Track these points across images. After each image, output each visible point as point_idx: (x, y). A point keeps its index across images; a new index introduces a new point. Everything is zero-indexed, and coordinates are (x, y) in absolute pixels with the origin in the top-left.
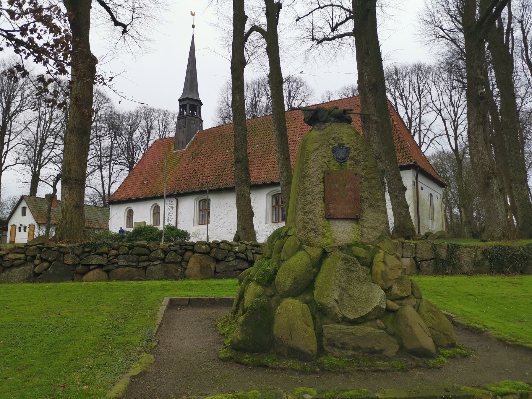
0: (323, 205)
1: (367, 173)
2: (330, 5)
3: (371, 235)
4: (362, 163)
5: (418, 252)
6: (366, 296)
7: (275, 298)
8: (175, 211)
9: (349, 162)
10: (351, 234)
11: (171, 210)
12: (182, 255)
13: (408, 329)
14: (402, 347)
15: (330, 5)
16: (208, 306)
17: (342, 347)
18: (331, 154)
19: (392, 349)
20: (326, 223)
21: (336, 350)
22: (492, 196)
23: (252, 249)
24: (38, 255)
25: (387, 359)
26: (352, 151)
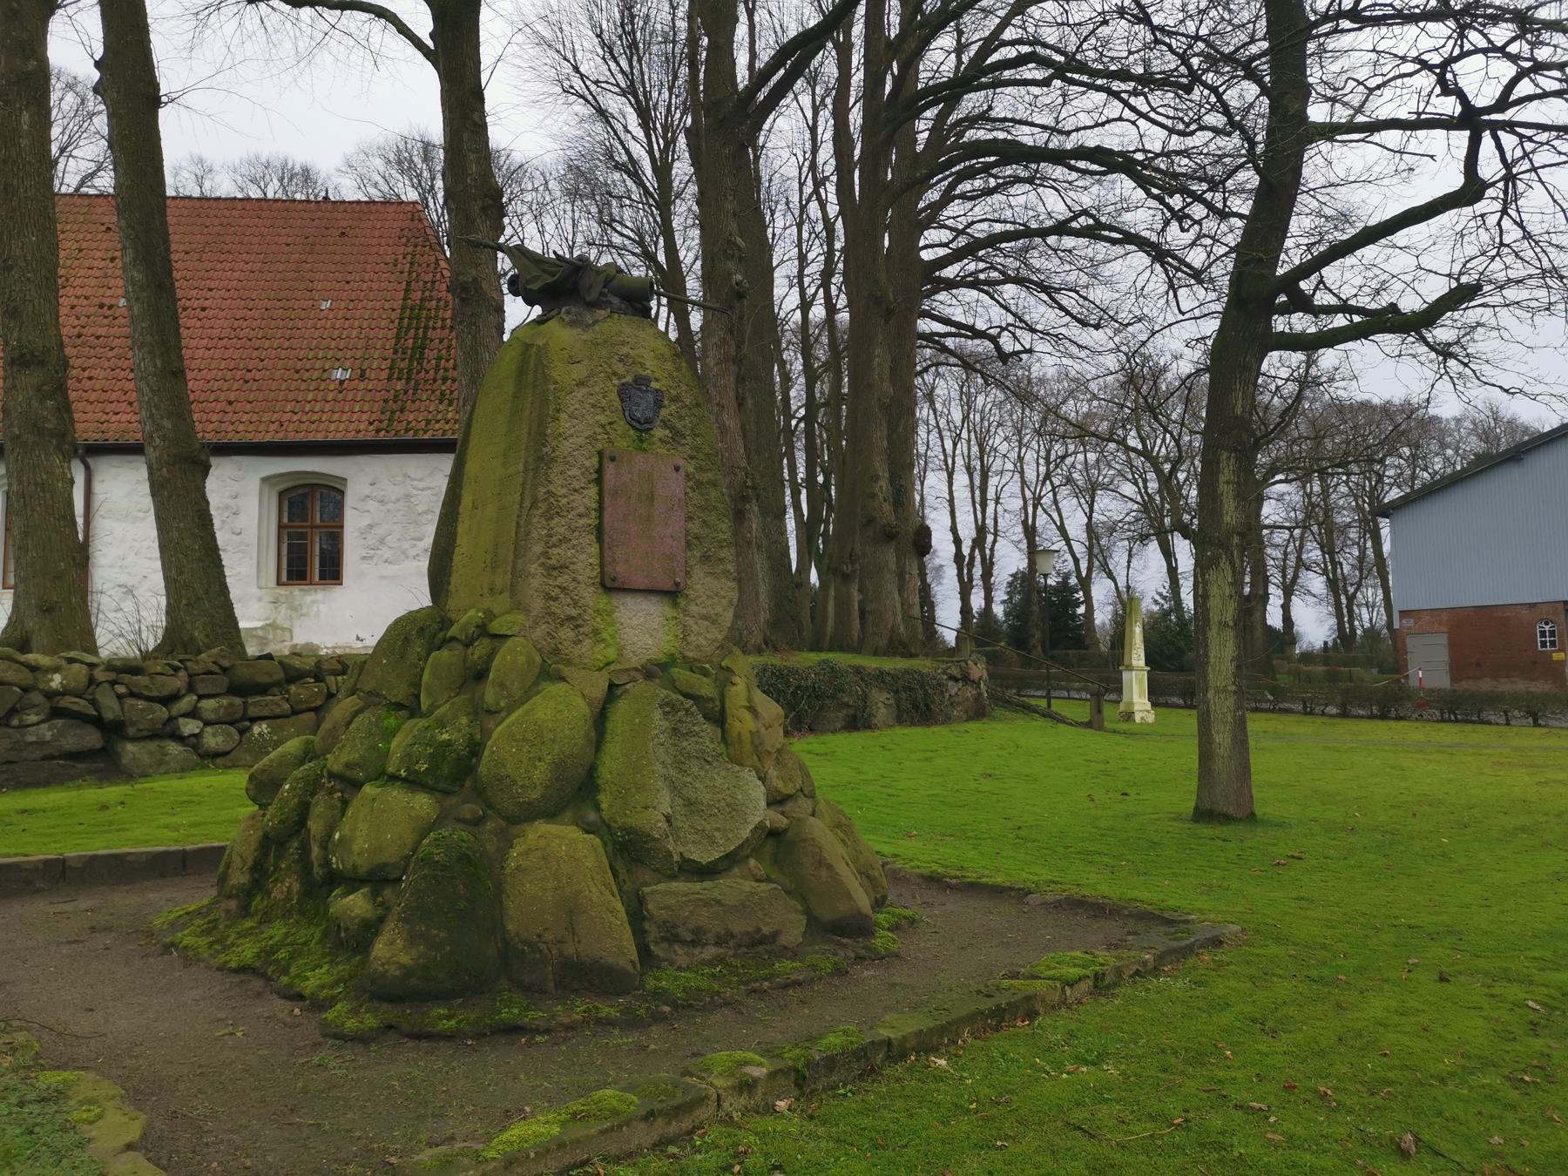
1: (699, 469)
2: (1362, 105)
4: (689, 440)
6: (729, 799)
7: (489, 826)
9: (659, 432)
10: (660, 635)
13: (824, 873)
14: (812, 921)
15: (1362, 105)
16: (38, 891)
17: (693, 941)
18: (617, 403)
19: (793, 930)
20: (603, 601)
21: (680, 951)
22: (749, 543)
23: (113, 683)
25: (793, 953)
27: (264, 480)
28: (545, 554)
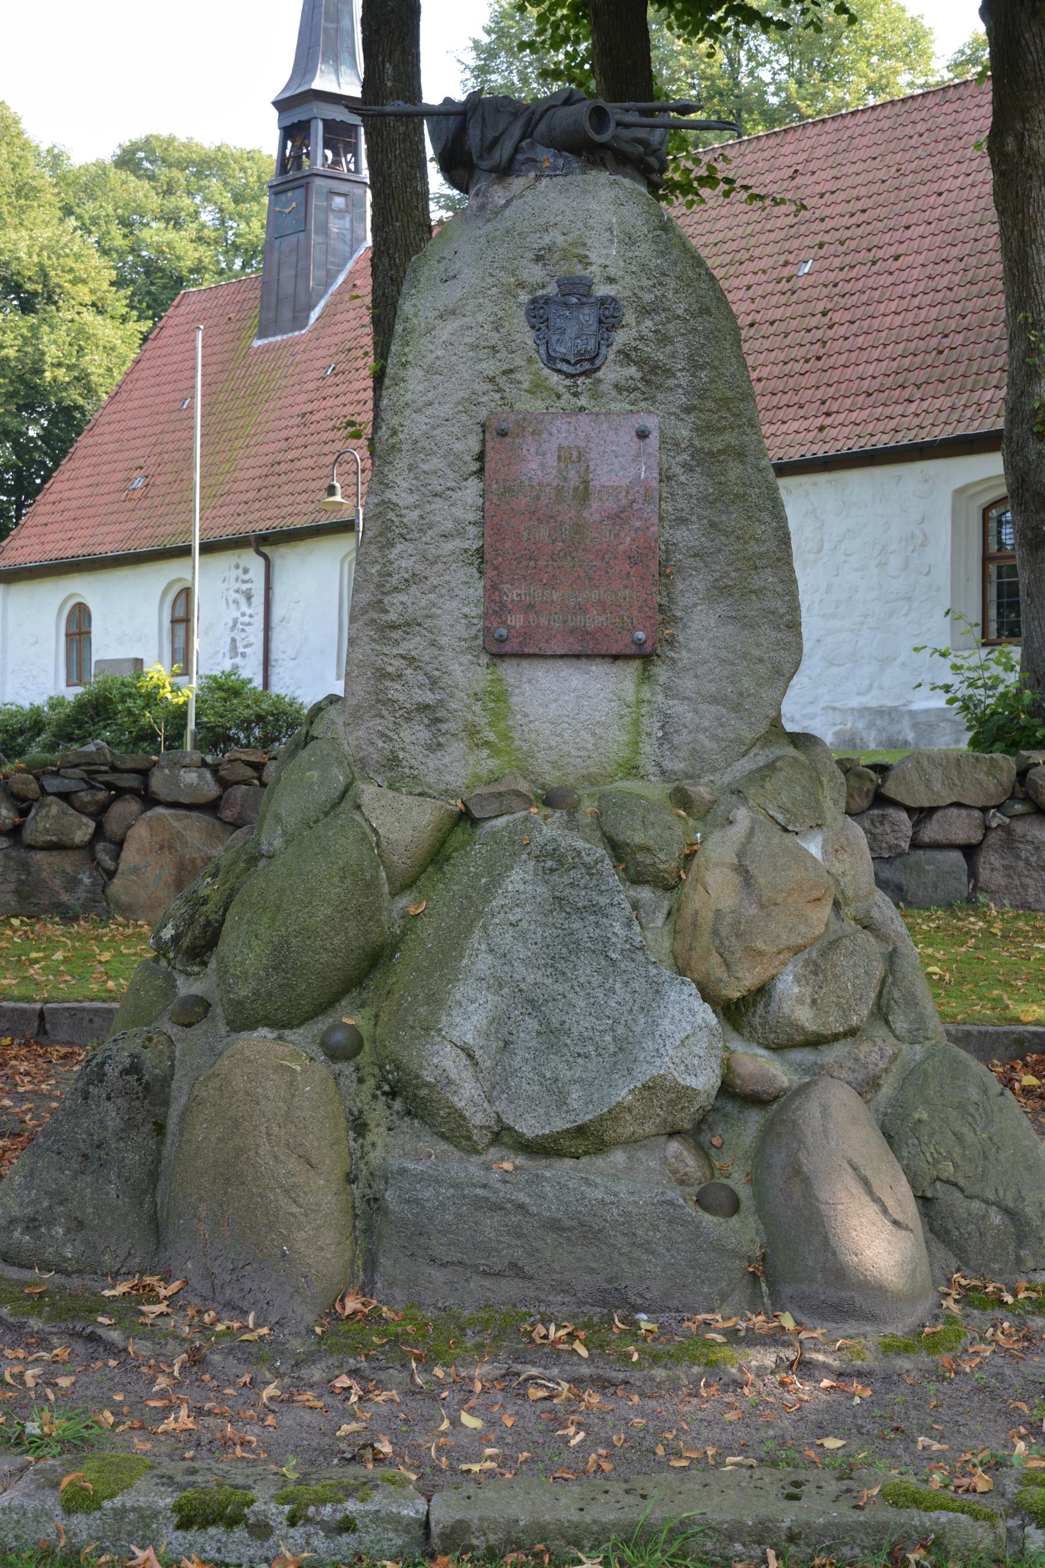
0: (477, 590)
1: (703, 430)
3: (715, 738)
4: (683, 378)
8: (261, 609)
11: (244, 608)
12: (99, 813)
18: (526, 337)
26: (630, 317)
27: (959, 492)
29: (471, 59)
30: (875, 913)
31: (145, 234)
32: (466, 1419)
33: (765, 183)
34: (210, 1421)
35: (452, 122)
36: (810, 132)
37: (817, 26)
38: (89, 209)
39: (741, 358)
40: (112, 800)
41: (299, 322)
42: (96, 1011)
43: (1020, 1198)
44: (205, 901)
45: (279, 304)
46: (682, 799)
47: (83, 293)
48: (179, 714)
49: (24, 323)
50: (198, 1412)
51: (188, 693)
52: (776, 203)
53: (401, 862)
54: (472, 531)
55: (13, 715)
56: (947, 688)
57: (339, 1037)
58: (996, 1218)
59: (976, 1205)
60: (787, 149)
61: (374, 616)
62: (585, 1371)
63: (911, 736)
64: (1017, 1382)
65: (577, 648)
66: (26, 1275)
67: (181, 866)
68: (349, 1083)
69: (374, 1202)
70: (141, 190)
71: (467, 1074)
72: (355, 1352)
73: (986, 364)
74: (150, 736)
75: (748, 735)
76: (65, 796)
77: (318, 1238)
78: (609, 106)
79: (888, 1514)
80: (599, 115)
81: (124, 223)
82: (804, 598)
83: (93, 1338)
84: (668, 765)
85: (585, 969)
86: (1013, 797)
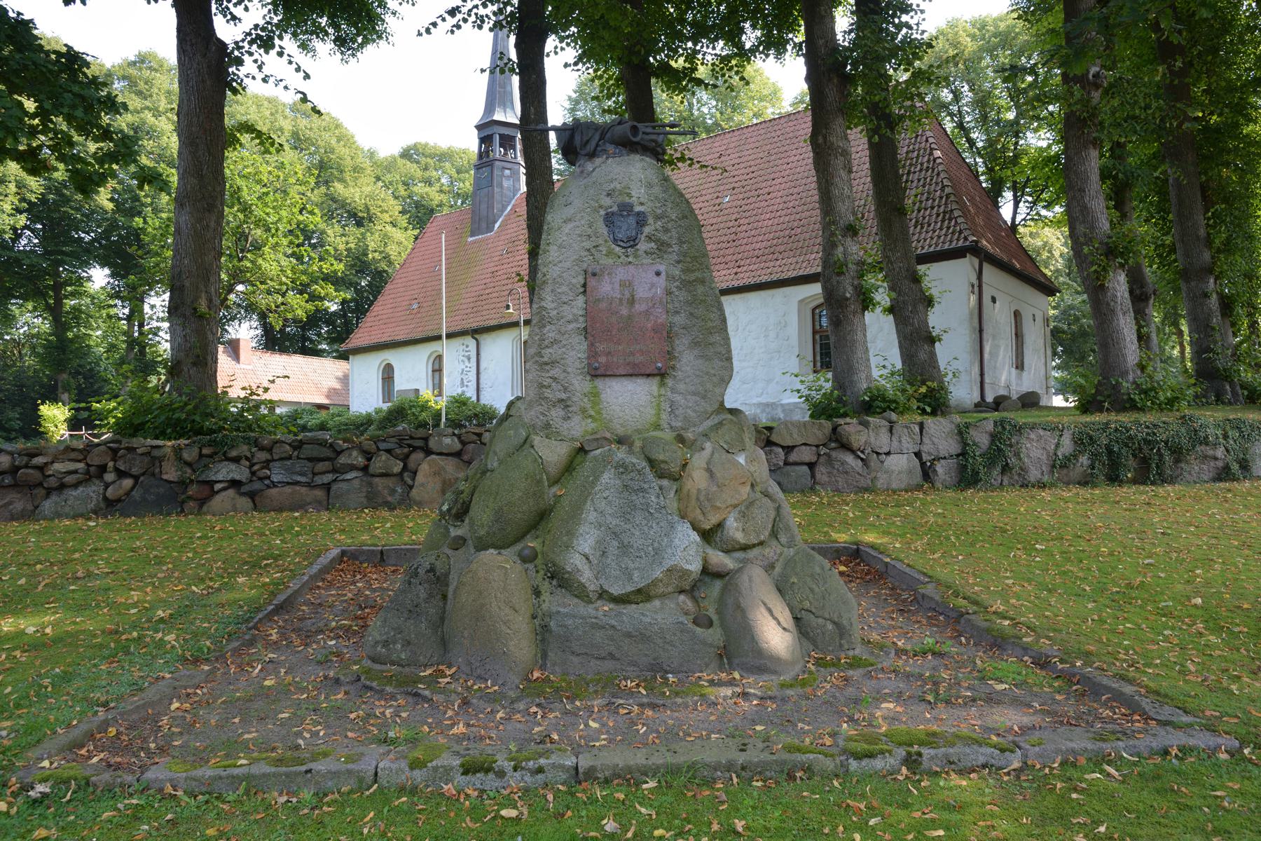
0: (584, 346)
3: (695, 411)
4: (676, 248)
5: (926, 440)
12: (405, 459)
18: (604, 230)
24: (111, 464)
26: (651, 221)
27: (801, 302)
28: (540, 355)
29: (567, 105)
30: (770, 490)
31: (415, 189)
32: (591, 723)
33: (706, 160)
34: (473, 729)
35: (568, 133)
36: (727, 136)
37: (731, 88)
38: (388, 177)
39: (703, 240)
40: (411, 452)
41: (490, 229)
42: (407, 550)
43: (840, 616)
44: (462, 492)
45: (480, 220)
46: (681, 439)
47: (386, 217)
48: (437, 415)
49: (358, 232)
50: (468, 725)
51: (442, 404)
52: (714, 169)
53: (553, 470)
54: (581, 319)
55: (357, 417)
56: (798, 391)
57: (526, 552)
58: (830, 626)
59: (820, 621)
60: (717, 144)
61: (535, 359)
62: (645, 700)
63: (782, 416)
64: (842, 699)
65: (631, 372)
66: (384, 667)
67: (444, 482)
68: (532, 573)
69: (545, 627)
70: (413, 168)
71: (586, 567)
72: (539, 696)
73: (812, 242)
74: (424, 425)
75: (710, 410)
76: (388, 451)
77: (521, 647)
78: (639, 125)
79: (786, 756)
80: (635, 130)
81: (405, 184)
82: (734, 353)
83: (416, 695)
84: (673, 424)
85: (639, 517)
86: (830, 440)
